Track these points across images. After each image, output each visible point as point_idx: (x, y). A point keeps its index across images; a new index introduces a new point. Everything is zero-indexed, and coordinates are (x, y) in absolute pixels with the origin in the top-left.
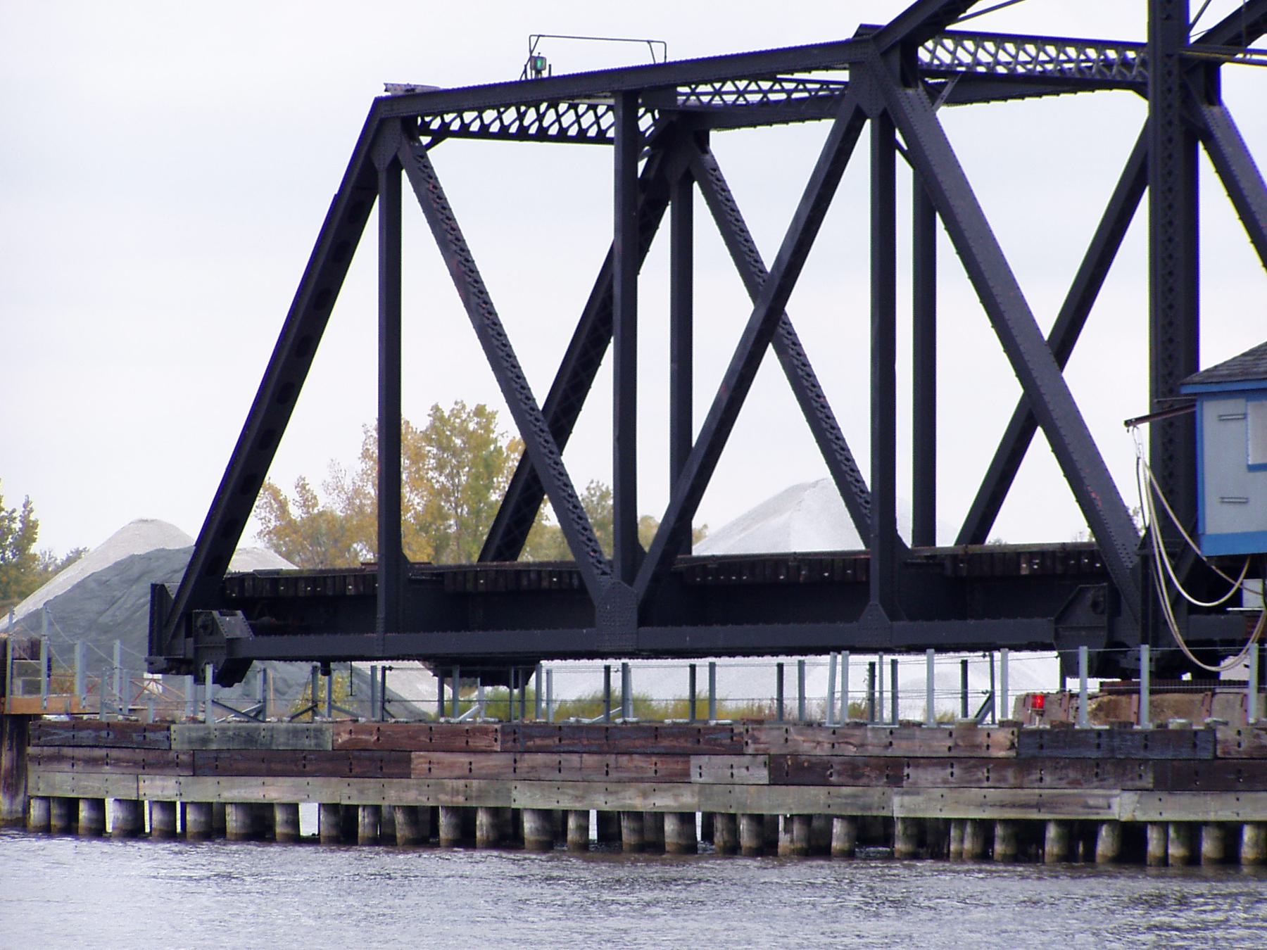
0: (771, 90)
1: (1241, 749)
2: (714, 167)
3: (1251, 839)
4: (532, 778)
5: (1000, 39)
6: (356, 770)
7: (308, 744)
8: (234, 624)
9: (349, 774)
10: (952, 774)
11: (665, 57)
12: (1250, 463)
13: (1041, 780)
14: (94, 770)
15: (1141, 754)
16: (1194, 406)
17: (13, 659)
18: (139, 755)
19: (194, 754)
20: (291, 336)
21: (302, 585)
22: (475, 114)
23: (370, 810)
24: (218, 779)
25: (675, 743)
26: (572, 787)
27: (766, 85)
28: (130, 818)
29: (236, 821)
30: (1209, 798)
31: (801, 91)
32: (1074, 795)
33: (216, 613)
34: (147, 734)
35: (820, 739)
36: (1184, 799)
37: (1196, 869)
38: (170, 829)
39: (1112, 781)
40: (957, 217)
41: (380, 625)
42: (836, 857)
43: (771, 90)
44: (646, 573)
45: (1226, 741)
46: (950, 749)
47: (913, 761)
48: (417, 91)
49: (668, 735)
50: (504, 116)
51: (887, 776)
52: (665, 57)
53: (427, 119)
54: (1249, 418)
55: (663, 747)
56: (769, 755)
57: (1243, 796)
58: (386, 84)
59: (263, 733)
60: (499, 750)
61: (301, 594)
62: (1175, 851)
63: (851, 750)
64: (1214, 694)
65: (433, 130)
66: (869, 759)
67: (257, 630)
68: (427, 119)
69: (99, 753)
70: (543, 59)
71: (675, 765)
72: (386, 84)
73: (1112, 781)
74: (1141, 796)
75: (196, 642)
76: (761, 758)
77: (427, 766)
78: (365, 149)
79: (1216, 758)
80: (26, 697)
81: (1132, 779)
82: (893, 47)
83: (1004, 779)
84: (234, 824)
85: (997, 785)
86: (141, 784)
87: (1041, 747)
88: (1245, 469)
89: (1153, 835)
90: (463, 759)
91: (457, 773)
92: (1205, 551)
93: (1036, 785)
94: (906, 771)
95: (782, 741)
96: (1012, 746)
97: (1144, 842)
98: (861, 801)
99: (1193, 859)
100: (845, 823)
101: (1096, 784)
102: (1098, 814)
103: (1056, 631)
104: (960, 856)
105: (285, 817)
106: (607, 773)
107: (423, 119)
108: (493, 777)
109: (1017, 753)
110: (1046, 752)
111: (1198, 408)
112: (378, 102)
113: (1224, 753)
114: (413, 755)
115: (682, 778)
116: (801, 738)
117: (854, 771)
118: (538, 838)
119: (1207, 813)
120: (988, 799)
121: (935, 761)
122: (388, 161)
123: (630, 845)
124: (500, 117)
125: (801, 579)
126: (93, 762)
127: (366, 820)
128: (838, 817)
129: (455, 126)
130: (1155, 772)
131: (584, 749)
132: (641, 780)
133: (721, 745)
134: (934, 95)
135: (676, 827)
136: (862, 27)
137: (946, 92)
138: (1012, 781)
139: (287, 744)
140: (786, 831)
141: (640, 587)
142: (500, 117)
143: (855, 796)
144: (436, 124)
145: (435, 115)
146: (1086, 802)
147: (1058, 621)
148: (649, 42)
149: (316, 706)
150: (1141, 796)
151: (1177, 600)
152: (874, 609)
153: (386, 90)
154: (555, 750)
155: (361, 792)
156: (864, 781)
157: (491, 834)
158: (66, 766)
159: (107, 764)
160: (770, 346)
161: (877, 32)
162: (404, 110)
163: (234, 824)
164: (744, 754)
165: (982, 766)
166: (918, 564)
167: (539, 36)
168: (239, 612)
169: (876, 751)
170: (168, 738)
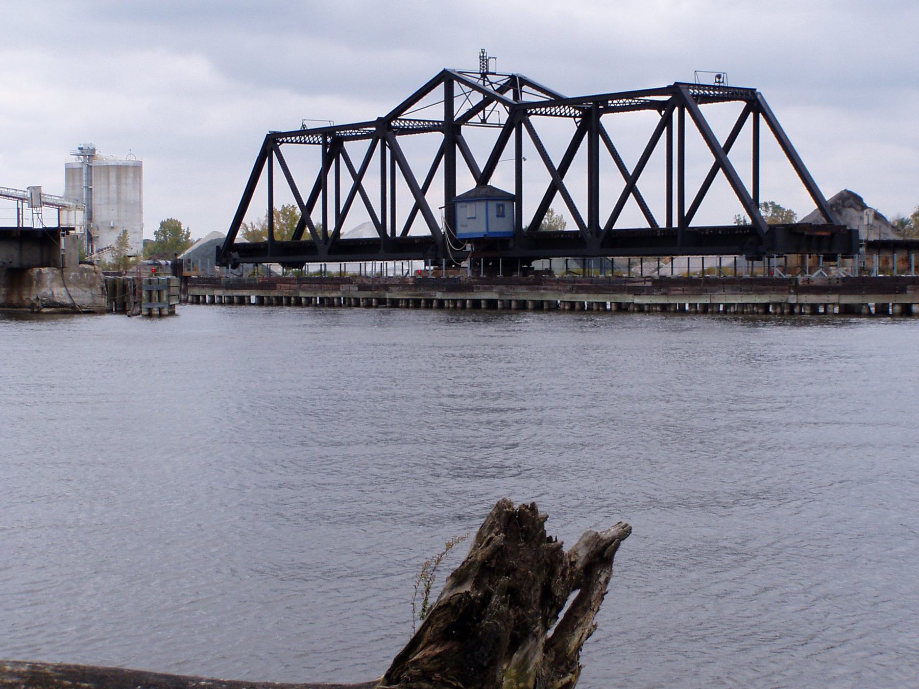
4: (304, 290)
8: (235, 255)
36: (453, 294)
44: (330, 242)
47: (391, 285)
63: (377, 283)
67: (241, 256)
89: (446, 303)
90: (288, 285)
108: (295, 289)
112: (267, 135)
115: (339, 289)
129: (285, 141)
134: (395, 133)
136: (379, 118)
144: (281, 140)
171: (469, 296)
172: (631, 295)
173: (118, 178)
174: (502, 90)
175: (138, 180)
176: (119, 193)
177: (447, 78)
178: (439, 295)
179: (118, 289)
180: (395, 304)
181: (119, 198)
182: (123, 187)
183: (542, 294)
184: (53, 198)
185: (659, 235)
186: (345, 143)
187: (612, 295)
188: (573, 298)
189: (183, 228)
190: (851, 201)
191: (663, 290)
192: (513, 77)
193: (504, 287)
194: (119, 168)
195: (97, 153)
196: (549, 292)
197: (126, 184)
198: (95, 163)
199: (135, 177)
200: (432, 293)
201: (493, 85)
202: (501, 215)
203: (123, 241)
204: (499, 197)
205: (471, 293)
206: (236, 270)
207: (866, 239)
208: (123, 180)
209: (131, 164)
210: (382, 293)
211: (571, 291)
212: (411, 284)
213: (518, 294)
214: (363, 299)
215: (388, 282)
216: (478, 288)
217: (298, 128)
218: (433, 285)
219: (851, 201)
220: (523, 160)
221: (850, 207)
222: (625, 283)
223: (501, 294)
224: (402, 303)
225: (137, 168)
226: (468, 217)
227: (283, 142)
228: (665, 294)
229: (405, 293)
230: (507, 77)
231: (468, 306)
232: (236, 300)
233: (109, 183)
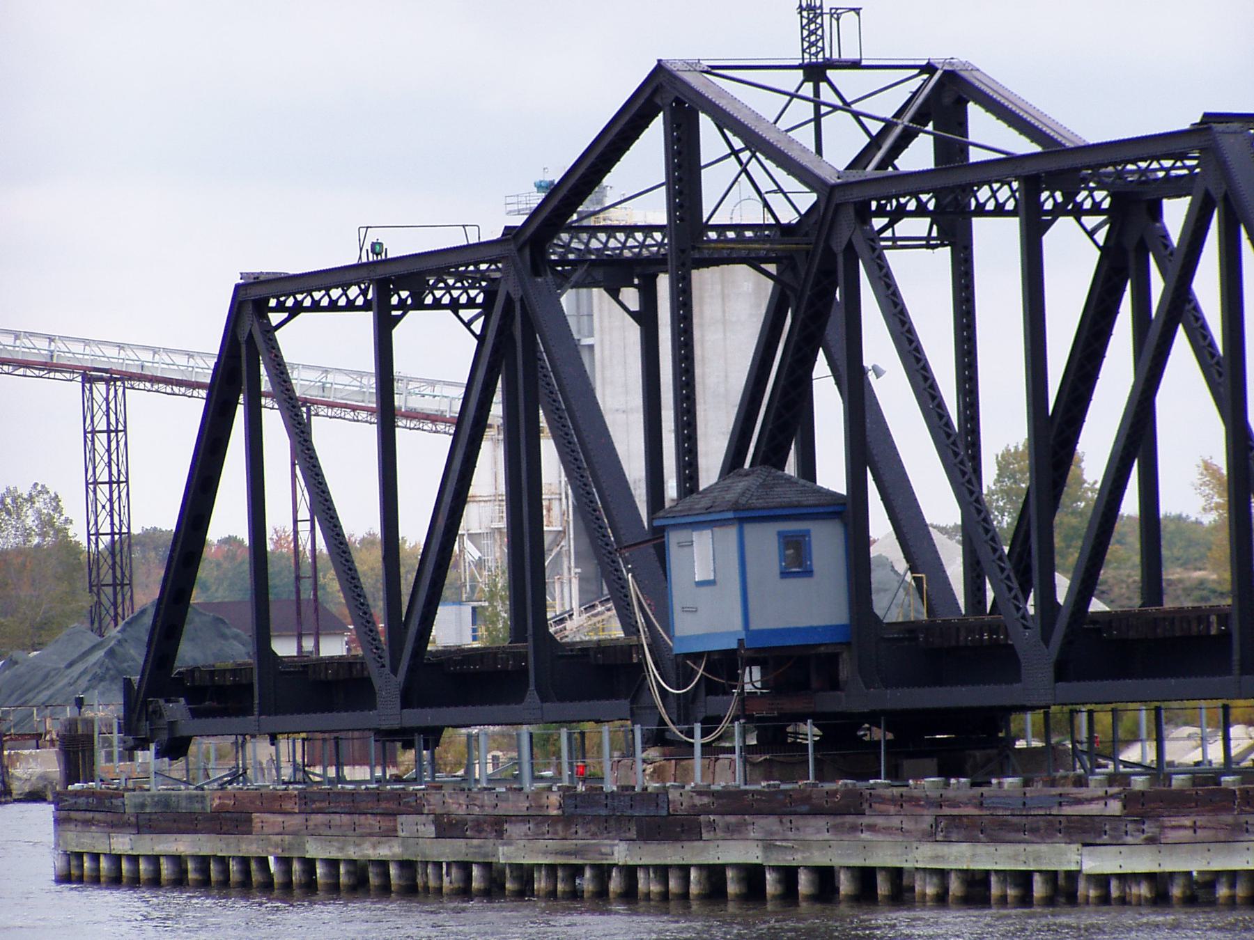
0: (1173, 167)
1: (683, 808)
2: (1164, 234)
3: (695, 877)
5: (630, 230)
6: (225, 828)
7: (197, 807)
8: (176, 710)
9: (219, 832)
10: (529, 828)
11: (479, 238)
12: (697, 580)
13: (576, 832)
14: (87, 829)
15: (629, 812)
16: (663, 537)
17: (100, 734)
18: (109, 817)
19: (137, 816)
20: (195, 476)
21: (228, 675)
22: (340, 291)
23: (237, 860)
24: (152, 836)
25: (388, 805)
26: (338, 841)
27: (1167, 163)
28: (113, 867)
29: (167, 869)
30: (666, 846)
31: (1179, 168)
32: (594, 844)
33: (161, 702)
34: (113, 800)
35: (461, 802)
36: (653, 847)
37: (722, 906)
38: (94, 874)
39: (614, 833)
41: (1236, 669)
42: (477, 896)
43: (1173, 167)
45: (674, 801)
46: (528, 808)
47: (508, 818)
48: (262, 278)
49: (388, 800)
50: (349, 292)
51: (496, 831)
52: (479, 238)
53: (903, 200)
54: (695, 544)
55: (383, 808)
56: (435, 814)
57: (687, 844)
58: (241, 274)
59: (173, 799)
60: (297, 811)
61: (228, 683)
62: (655, 888)
63: (477, 810)
64: (717, 759)
65: (289, 307)
66: (487, 817)
67: (195, 714)
68: (903, 200)
69: (89, 815)
70: (381, 244)
71: (386, 823)
72: (241, 274)
73: (614, 833)
74: (629, 845)
75: (151, 725)
76: (431, 817)
77: (260, 824)
78: (232, 324)
79: (669, 814)
80: (108, 764)
81: (625, 832)
82: (525, 244)
83: (556, 833)
84: (166, 872)
85: (554, 837)
86: (112, 840)
87: (576, 807)
88: (694, 585)
89: (641, 875)
90: (279, 818)
91: (277, 830)
92: (678, 649)
93: (574, 837)
94: (506, 826)
95: (442, 802)
96: (560, 807)
98: (483, 850)
99: (602, 893)
100: (735, 871)
101: (605, 835)
102: (607, 859)
103: (631, 709)
104: (1087, 902)
105: (194, 866)
106: (355, 830)
107: (898, 201)
108: (295, 834)
109: (563, 812)
110: (579, 811)
111: (666, 539)
112: (237, 287)
113: (673, 810)
114: (254, 815)
115: (391, 833)
116: (451, 801)
118: (329, 881)
119: (666, 858)
120: (549, 848)
121: (520, 818)
122: (246, 335)
123: (375, 886)
124: (345, 293)
125: (510, 668)
126: (88, 823)
127: (235, 868)
128: (476, 863)
129: (307, 302)
130: (637, 826)
131: (343, 810)
132: (371, 835)
133: (411, 807)
134: (564, 281)
135: (397, 872)
136: (507, 228)
137: (574, 278)
138: (561, 834)
139: (186, 809)
140: (448, 874)
142: (345, 293)
143: (480, 847)
144: (290, 302)
145: (288, 296)
146: (600, 851)
147: (632, 702)
148: (464, 226)
149: (245, 773)
150: (629, 845)
151: (663, 692)
152: (532, 696)
153: (839, 178)
154: (327, 811)
155: (228, 845)
156: (484, 834)
157: (303, 879)
158: (72, 827)
159: (93, 825)
161: (515, 232)
162: (256, 293)
163: (166, 872)
164: (423, 814)
165: (545, 822)
166: (290, 673)
167: (368, 227)
168: (182, 700)
169: (488, 811)
170: (123, 803)
172: (1074, 847)
178: (620, 853)
179: (1074, 706)
184: (438, 391)
185: (1213, 631)
187: (1030, 848)
188: (936, 858)
193: (771, 822)
196: (880, 837)
197: (724, 322)
200: (605, 844)
201: (840, 104)
203: (1204, 484)
204: (791, 506)
205: (696, 843)
206: (181, 763)
211: (930, 836)
212: (555, 812)
213: (806, 844)
214: (449, 864)
216: (712, 826)
218: (607, 819)
220: (871, 376)
222: (1060, 804)
223: (768, 845)
224: (540, 881)
227: (297, 309)
228: (1152, 841)
230: (916, 71)
232: (166, 869)
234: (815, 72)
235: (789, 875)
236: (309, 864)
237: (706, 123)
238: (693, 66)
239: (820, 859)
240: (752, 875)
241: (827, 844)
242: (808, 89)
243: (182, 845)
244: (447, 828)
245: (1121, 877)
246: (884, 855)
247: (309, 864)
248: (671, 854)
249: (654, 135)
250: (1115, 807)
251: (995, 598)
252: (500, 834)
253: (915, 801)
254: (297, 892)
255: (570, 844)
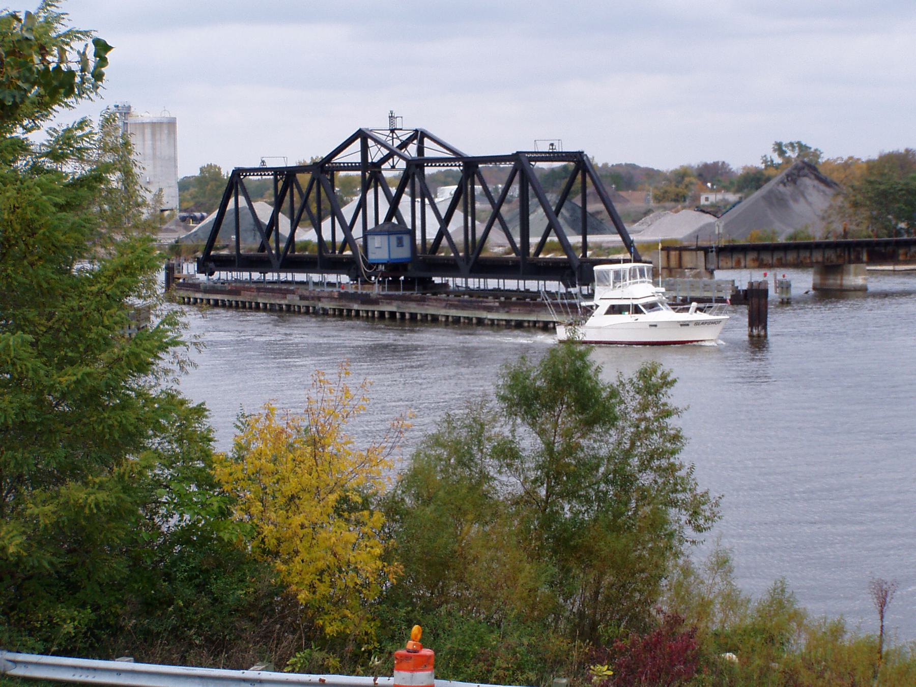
4: (261, 297)
8: (212, 265)
40: (900, 151)
44: (281, 258)
47: (323, 297)
62: (365, 315)
89: (361, 312)
97: (384, 315)
108: (255, 296)
117: (313, 298)
141: (280, 260)
160: (394, 195)
171: (377, 308)
173: (153, 134)
174: (404, 145)
175: (173, 135)
176: (154, 149)
177: (362, 135)
178: (356, 307)
180: (325, 313)
181: (154, 155)
182: (158, 143)
183: (427, 309)
186: (298, 175)
189: (223, 173)
190: (806, 171)
191: (506, 309)
192: (416, 131)
193: (399, 303)
194: (153, 125)
195: (132, 109)
198: (130, 120)
199: (169, 134)
200: (351, 304)
202: (400, 244)
207: (717, 245)
208: (158, 137)
209: (165, 120)
210: (316, 302)
211: (445, 307)
213: (409, 308)
215: (320, 295)
217: (257, 165)
219: (806, 171)
221: (805, 176)
223: (398, 307)
225: (171, 124)
226: (376, 246)
228: (507, 312)
229: (332, 303)
231: (376, 316)
233: (144, 140)
234: (392, 131)
235: (403, 314)
236: (189, 298)
237: (369, 140)
238: (368, 129)
239: (413, 311)
240: (392, 314)
241: (415, 308)
242: (391, 135)
243: (218, 297)
244: (303, 298)
245: (498, 320)
246: (431, 311)
247: (299, 307)
248: (370, 308)
249: (358, 143)
250: (497, 304)
251: (268, 239)
252: (320, 300)
253: (440, 300)
254: (376, 320)
255: (341, 304)
